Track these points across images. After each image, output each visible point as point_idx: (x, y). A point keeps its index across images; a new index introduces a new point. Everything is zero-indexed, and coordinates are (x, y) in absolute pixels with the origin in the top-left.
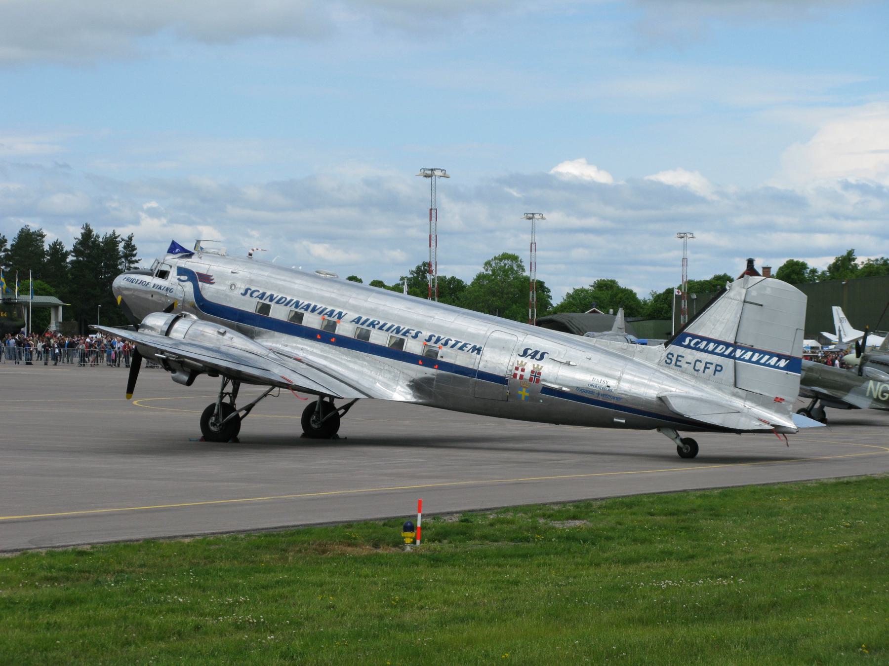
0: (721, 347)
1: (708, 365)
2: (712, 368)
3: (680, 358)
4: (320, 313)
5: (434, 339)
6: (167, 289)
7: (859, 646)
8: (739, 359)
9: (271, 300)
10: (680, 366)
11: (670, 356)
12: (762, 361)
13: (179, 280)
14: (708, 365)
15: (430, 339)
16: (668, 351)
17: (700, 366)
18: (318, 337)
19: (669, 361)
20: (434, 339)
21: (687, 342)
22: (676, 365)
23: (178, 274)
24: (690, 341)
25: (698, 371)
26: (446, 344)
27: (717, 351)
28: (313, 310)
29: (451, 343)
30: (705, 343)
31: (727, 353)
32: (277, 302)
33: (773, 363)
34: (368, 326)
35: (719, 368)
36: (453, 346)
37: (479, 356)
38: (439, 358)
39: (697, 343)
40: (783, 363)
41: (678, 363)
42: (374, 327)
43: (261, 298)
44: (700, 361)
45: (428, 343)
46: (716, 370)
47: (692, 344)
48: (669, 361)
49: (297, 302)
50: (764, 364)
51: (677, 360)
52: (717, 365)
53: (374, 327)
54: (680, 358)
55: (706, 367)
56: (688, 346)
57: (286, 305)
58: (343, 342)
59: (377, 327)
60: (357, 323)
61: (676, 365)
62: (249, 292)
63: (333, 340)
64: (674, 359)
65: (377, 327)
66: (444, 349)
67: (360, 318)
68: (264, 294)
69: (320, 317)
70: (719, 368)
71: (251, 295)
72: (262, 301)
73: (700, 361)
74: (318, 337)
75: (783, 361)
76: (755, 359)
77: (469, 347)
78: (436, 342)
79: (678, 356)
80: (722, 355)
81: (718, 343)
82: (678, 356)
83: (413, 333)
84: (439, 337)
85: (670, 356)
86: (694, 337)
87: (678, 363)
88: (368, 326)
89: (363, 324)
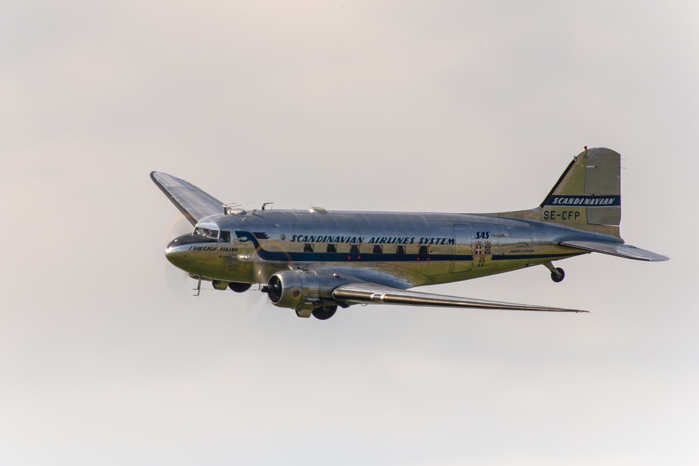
0: (577, 199)
1: (571, 214)
2: (573, 215)
3: (553, 213)
4: (347, 242)
5: (424, 241)
6: (233, 250)
7: (225, 236)
8: (588, 205)
9: (313, 241)
10: (554, 219)
11: (547, 213)
12: (600, 203)
13: (240, 241)
14: (571, 214)
15: (421, 242)
16: (544, 211)
17: (566, 215)
18: (349, 258)
19: (546, 217)
20: (424, 241)
21: (555, 202)
22: (551, 218)
23: (238, 237)
24: (558, 200)
25: (565, 219)
26: (432, 242)
27: (575, 203)
28: (342, 241)
29: (435, 241)
30: (567, 199)
31: (580, 203)
32: (318, 241)
33: (571, 203)
34: (381, 242)
35: (577, 214)
36: (437, 243)
37: (454, 246)
38: (430, 253)
39: (563, 201)
40: (611, 201)
41: (553, 217)
42: (384, 242)
43: (306, 241)
44: (566, 212)
45: (421, 245)
46: (576, 216)
47: (559, 203)
48: (546, 217)
49: (330, 237)
50: (602, 205)
51: (552, 215)
52: (576, 212)
53: (384, 242)
54: (553, 213)
55: (570, 215)
56: (557, 204)
57: (324, 241)
58: (366, 258)
59: (386, 241)
60: (373, 242)
61: (551, 218)
62: (296, 238)
63: (359, 257)
64: (549, 214)
65: (386, 241)
66: (432, 246)
67: (373, 239)
68: (306, 237)
69: (348, 244)
70: (577, 214)
71: (298, 240)
72: (307, 243)
73: (566, 212)
74: (349, 258)
75: (611, 199)
76: (592, 203)
77: (447, 241)
78: (426, 243)
79: (552, 212)
80: (578, 205)
81: (575, 197)
82: (552, 212)
83: (410, 240)
84: (426, 239)
85: (547, 213)
86: (559, 197)
87: (553, 217)
88: (381, 242)
89: (377, 242)
